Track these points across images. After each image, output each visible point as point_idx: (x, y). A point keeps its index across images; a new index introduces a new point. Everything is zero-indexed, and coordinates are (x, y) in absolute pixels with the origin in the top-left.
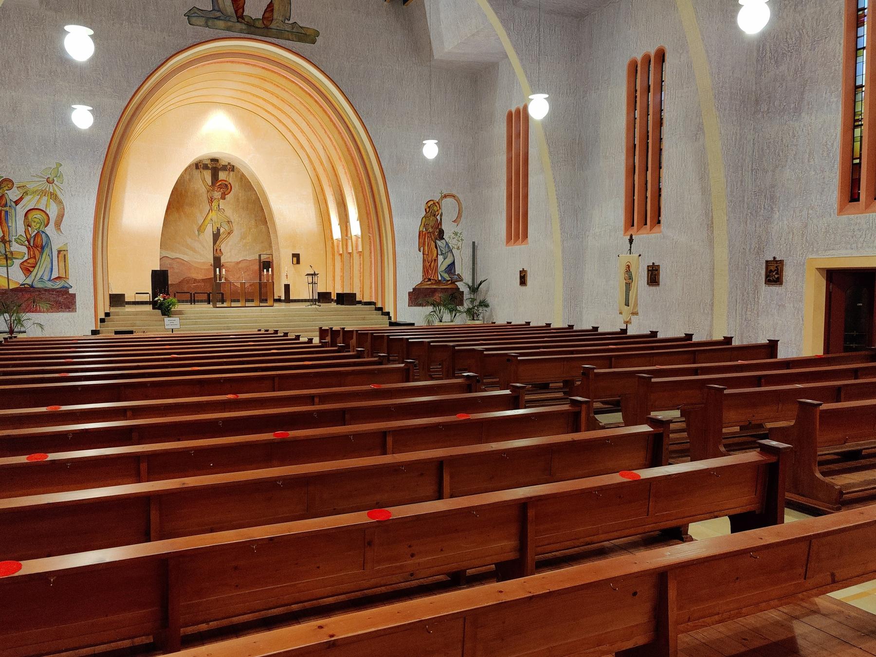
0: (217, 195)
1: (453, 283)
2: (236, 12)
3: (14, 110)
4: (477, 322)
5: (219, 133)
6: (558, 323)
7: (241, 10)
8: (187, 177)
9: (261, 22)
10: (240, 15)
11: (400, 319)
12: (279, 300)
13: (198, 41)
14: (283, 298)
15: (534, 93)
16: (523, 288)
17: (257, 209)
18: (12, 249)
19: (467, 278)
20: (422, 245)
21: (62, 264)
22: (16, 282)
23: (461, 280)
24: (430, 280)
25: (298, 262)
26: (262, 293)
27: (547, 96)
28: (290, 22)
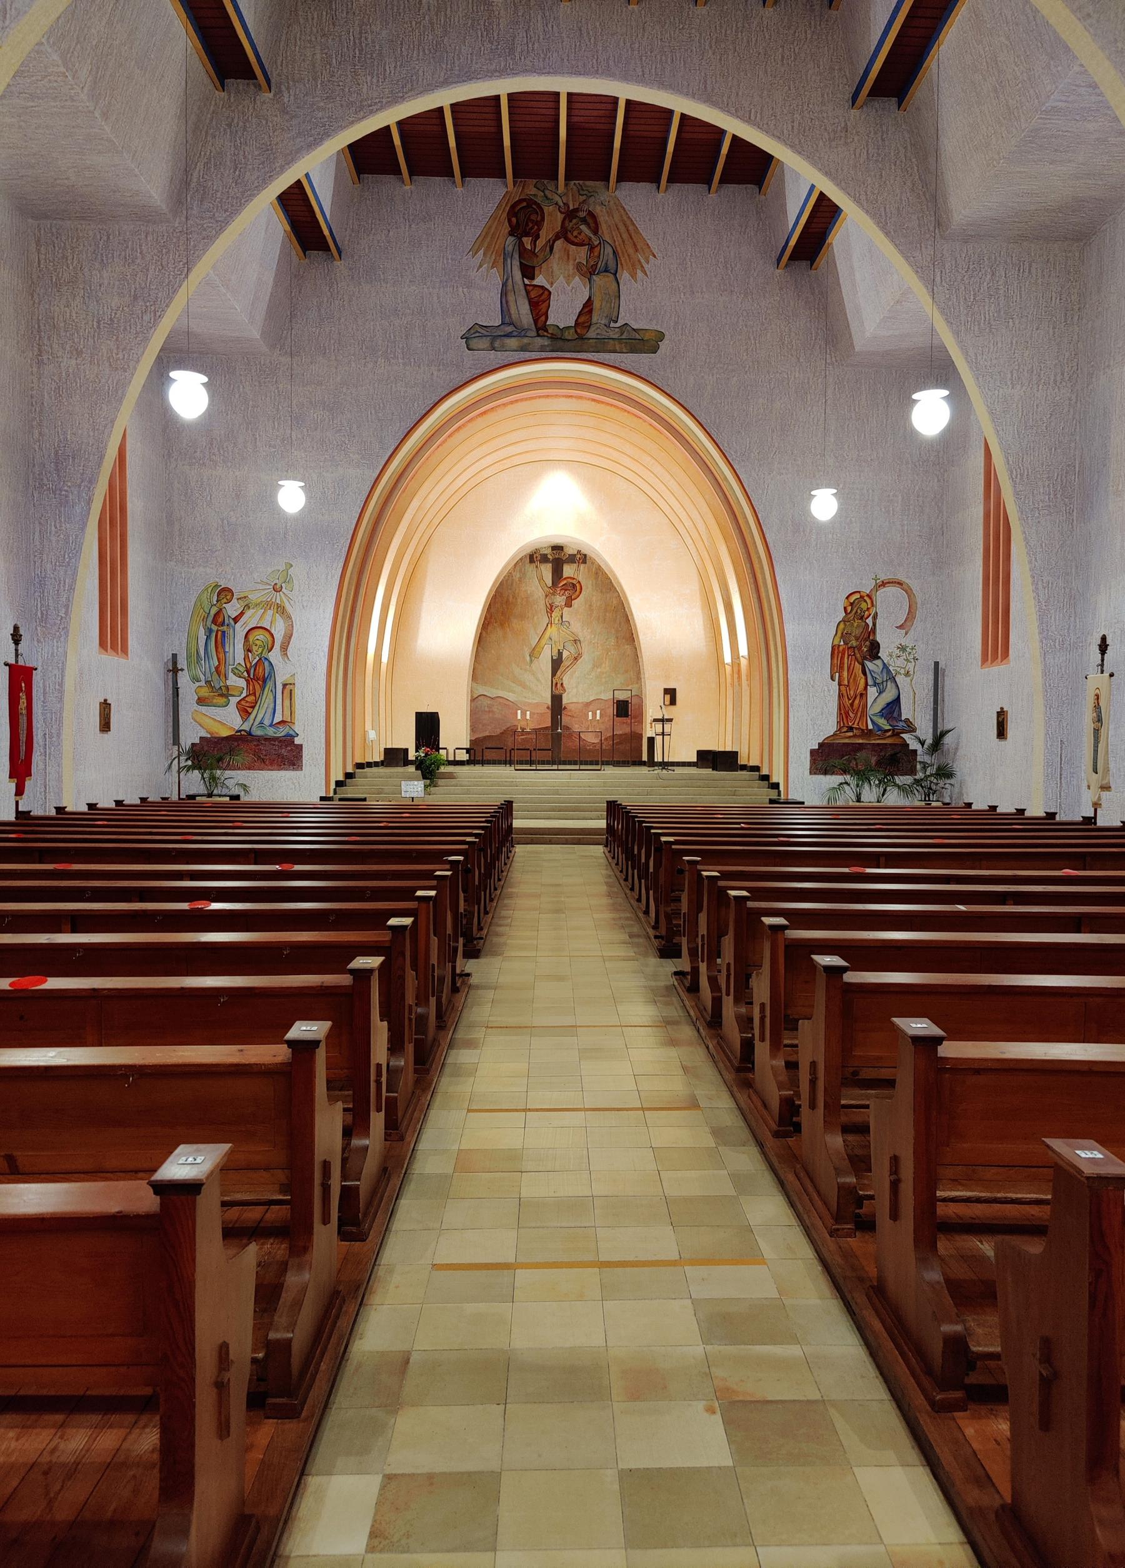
0: (560, 600)
1: (896, 734)
2: (536, 322)
3: (238, 496)
5: (556, 507)
6: (1036, 810)
7: (543, 318)
8: (517, 575)
9: (573, 330)
10: (541, 325)
11: (793, 796)
12: (643, 764)
13: (479, 371)
16: (1003, 743)
18: (228, 683)
20: (836, 668)
21: (287, 703)
24: (851, 729)
25: (673, 702)
27: (946, 393)
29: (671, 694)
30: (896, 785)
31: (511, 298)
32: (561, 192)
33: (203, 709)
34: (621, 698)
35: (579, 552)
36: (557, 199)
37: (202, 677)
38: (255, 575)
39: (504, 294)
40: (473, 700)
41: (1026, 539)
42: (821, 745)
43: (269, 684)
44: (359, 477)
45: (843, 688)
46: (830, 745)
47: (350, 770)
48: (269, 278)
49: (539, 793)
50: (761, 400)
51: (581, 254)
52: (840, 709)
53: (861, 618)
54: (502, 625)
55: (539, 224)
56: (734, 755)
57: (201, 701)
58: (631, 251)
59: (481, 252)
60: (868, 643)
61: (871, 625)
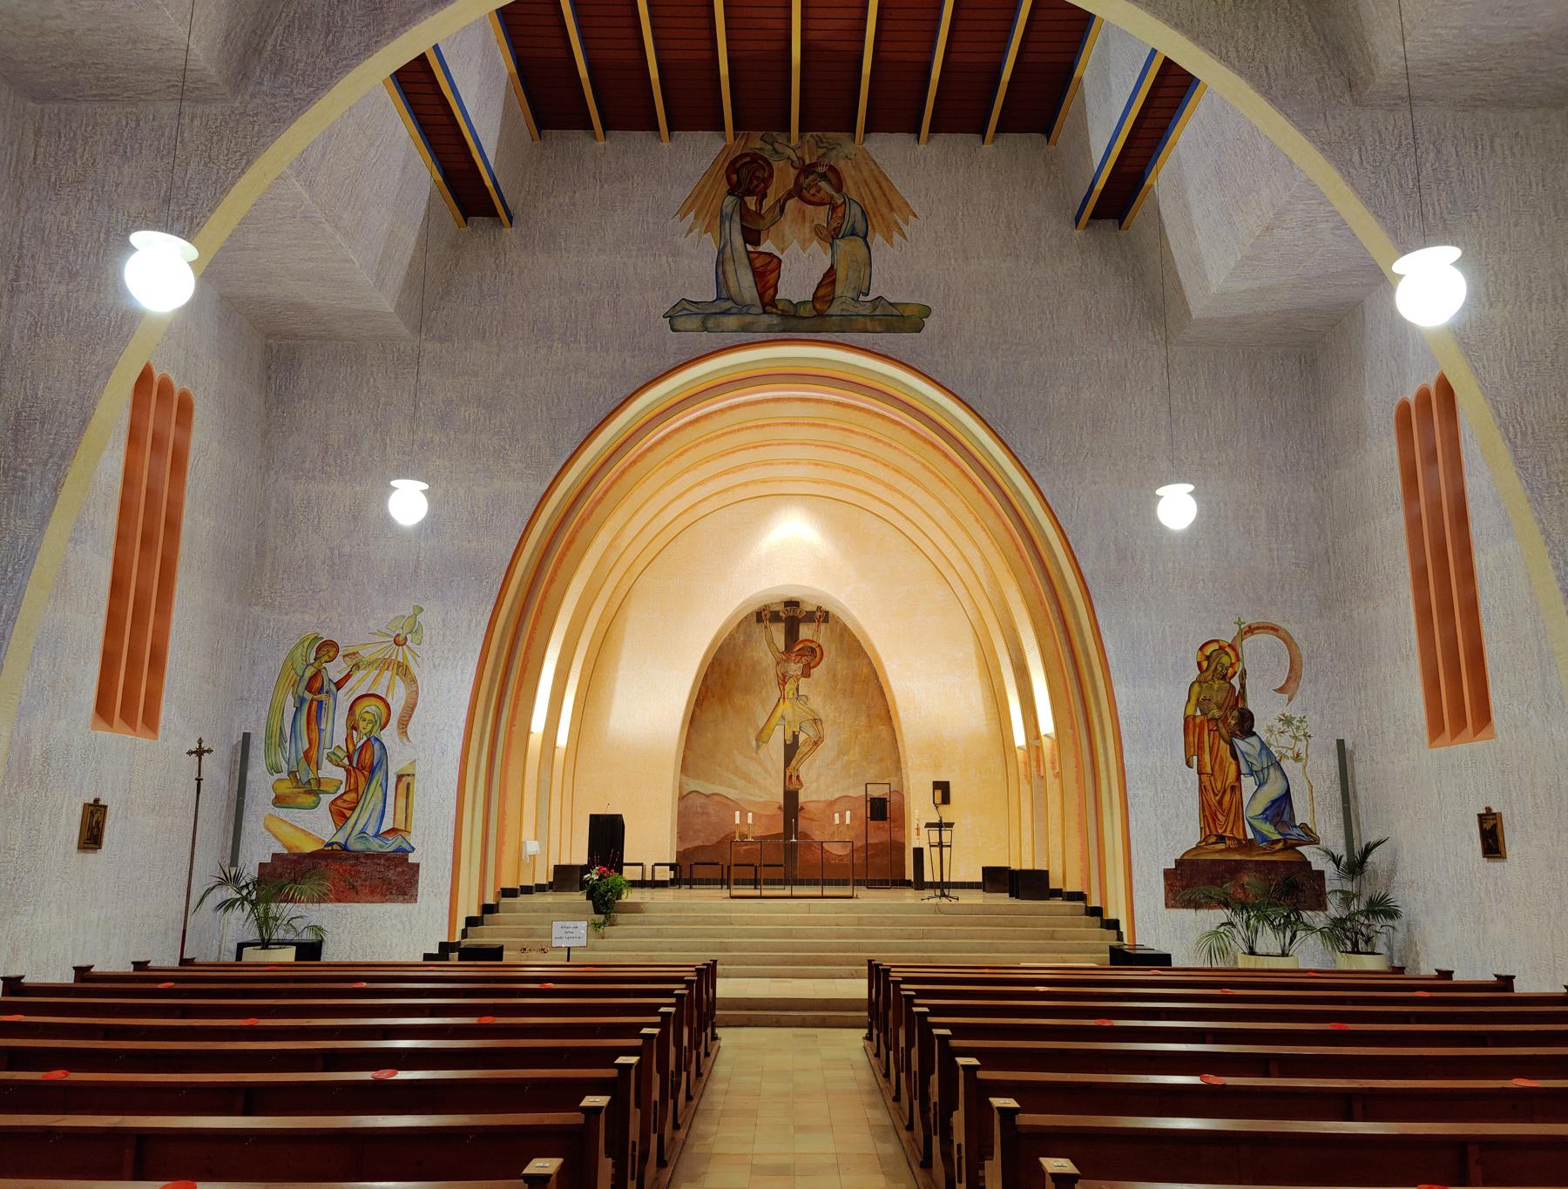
0: (795, 668)
1: (1290, 847)
2: (761, 295)
4: (1369, 963)
5: (790, 550)
7: (771, 291)
9: (810, 306)
12: (908, 884)
13: (685, 358)
15: (1405, 249)
16: (1496, 866)
18: (321, 774)
19: (1331, 835)
20: (1193, 749)
21: (402, 802)
22: (320, 840)
23: (1313, 840)
24: (1221, 839)
25: (946, 800)
26: (883, 862)
28: (869, 298)
29: (943, 788)
30: (1309, 928)
31: (729, 267)
32: (795, 144)
33: (282, 813)
34: (876, 795)
35: (819, 608)
36: (789, 152)
37: (284, 766)
38: (371, 624)
39: (720, 262)
40: (682, 798)
41: (1544, 531)
42: (1179, 863)
43: (379, 776)
44: (520, 490)
45: (1205, 778)
46: (1193, 863)
47: (490, 900)
48: (409, 237)
49: (755, 939)
50: (1063, 389)
51: (821, 215)
52: (1202, 808)
53: (1224, 677)
54: (721, 699)
55: (767, 181)
56: (1042, 876)
57: (279, 801)
58: (885, 210)
59: (692, 214)
60: (1235, 713)
61: (1238, 687)
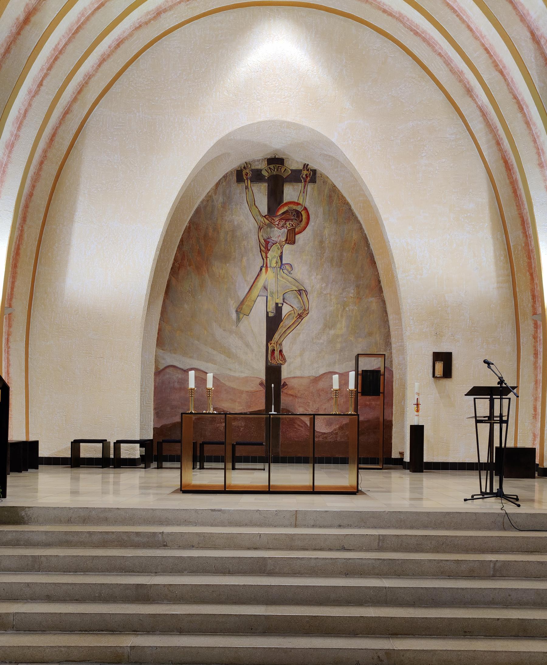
0: (278, 234)
8: (219, 199)
12: (399, 463)
14: (407, 459)
17: (361, 262)
25: (447, 373)
26: (368, 437)
35: (306, 166)
40: (158, 373)
